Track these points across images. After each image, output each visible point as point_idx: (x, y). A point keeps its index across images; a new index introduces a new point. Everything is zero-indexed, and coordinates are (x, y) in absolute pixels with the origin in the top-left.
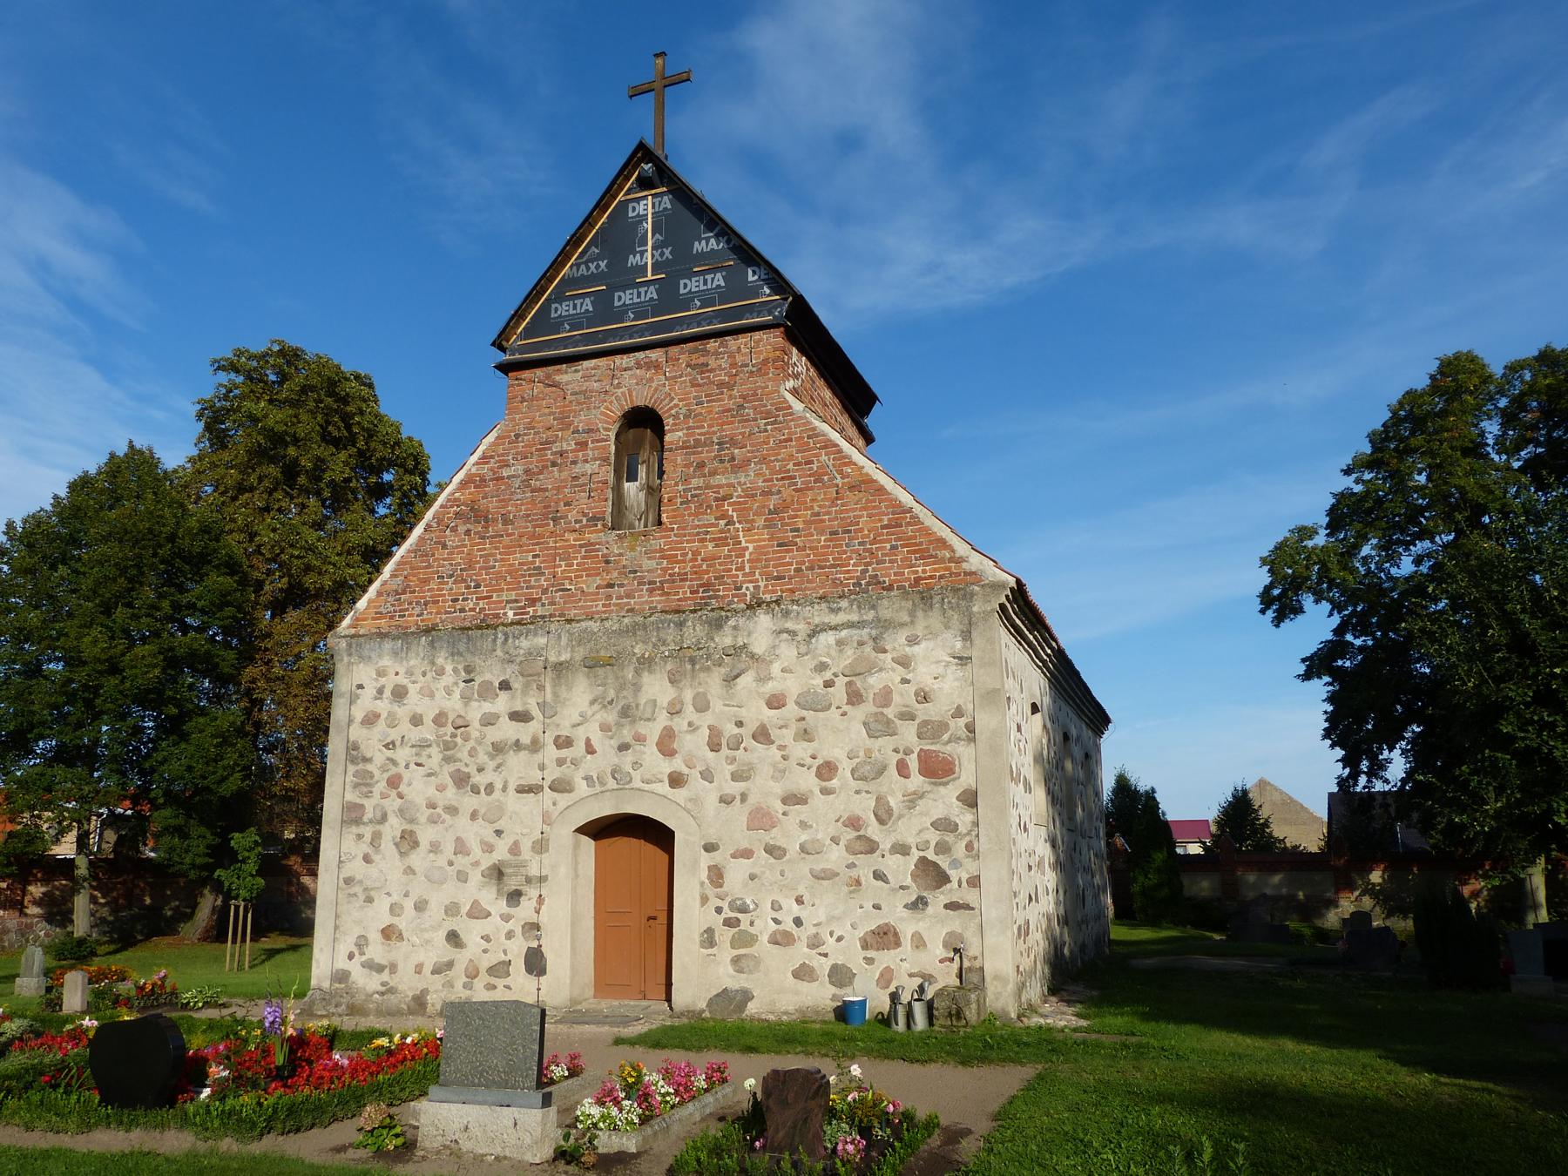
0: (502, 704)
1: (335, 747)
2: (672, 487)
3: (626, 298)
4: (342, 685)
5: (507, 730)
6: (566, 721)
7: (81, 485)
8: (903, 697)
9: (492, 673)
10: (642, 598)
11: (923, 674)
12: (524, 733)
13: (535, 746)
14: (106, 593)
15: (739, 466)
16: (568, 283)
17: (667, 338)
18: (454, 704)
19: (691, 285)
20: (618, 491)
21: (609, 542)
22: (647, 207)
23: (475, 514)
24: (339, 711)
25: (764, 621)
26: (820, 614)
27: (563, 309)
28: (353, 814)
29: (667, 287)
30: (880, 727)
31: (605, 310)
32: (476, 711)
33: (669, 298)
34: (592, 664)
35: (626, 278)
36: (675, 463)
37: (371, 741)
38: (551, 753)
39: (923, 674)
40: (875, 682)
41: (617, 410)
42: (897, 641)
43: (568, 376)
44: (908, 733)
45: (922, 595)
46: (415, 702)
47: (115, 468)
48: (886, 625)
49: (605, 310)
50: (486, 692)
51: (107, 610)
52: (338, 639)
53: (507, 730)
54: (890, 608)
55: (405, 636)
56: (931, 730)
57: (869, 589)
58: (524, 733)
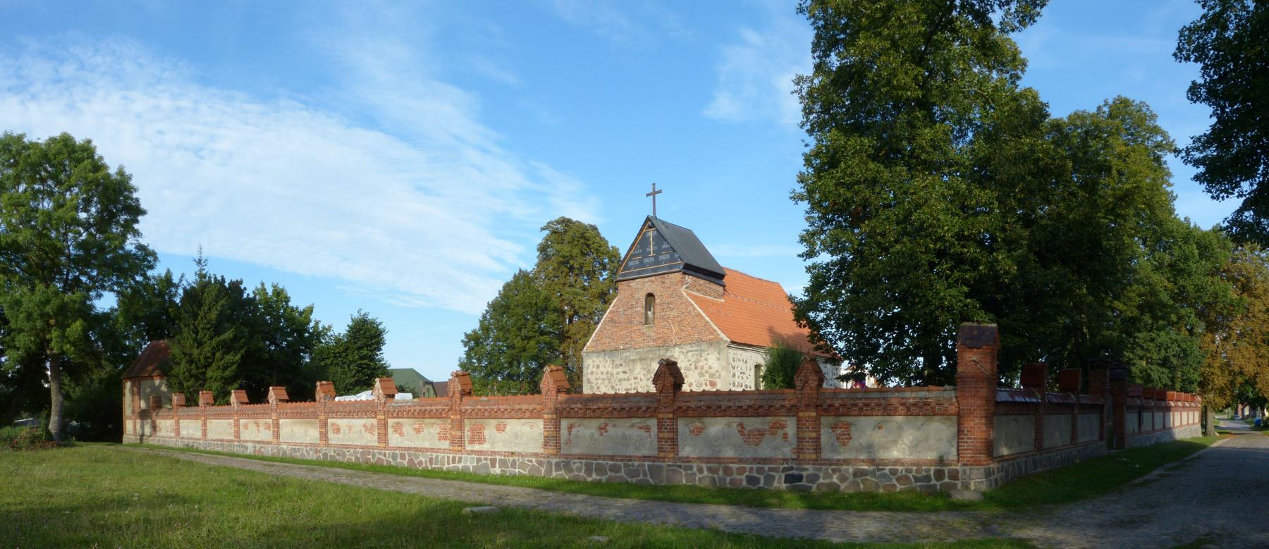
0: (620, 369)
1: (585, 379)
2: (657, 315)
3: (646, 260)
4: (585, 364)
5: (622, 376)
6: (636, 372)
7: (507, 287)
8: (706, 368)
9: (618, 362)
10: (652, 343)
11: (710, 362)
12: (626, 376)
13: (628, 379)
14: (519, 324)
15: (672, 310)
16: (633, 256)
17: (656, 273)
18: (610, 369)
19: (662, 258)
20: (646, 314)
21: (644, 328)
22: (651, 234)
23: (612, 321)
24: (585, 371)
25: (677, 349)
26: (689, 348)
27: (631, 263)
28: (713, 384)
29: (656, 258)
30: (701, 375)
31: (642, 264)
32: (615, 371)
33: (657, 261)
34: (641, 359)
35: (646, 254)
36: (658, 309)
37: (592, 378)
38: (633, 381)
39: (710, 362)
40: (700, 364)
41: (644, 294)
42: (705, 354)
43: (633, 284)
44: (707, 376)
45: (710, 343)
46: (601, 369)
47: (516, 278)
48: (702, 351)
49: (642, 264)
50: (617, 367)
51: (519, 329)
52: (583, 353)
53: (622, 376)
54: (704, 346)
55: (598, 352)
56: (712, 375)
57: (699, 342)
58: (626, 376)
